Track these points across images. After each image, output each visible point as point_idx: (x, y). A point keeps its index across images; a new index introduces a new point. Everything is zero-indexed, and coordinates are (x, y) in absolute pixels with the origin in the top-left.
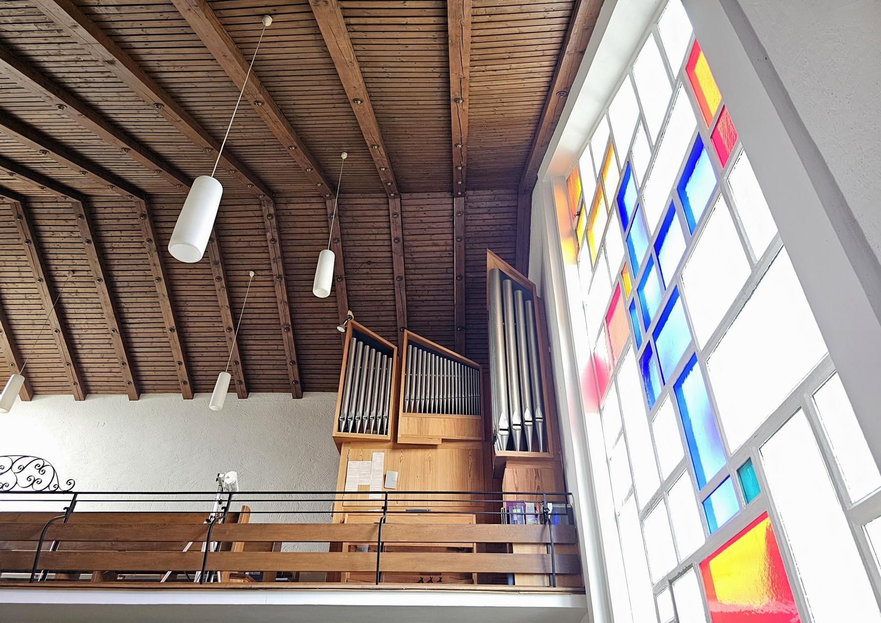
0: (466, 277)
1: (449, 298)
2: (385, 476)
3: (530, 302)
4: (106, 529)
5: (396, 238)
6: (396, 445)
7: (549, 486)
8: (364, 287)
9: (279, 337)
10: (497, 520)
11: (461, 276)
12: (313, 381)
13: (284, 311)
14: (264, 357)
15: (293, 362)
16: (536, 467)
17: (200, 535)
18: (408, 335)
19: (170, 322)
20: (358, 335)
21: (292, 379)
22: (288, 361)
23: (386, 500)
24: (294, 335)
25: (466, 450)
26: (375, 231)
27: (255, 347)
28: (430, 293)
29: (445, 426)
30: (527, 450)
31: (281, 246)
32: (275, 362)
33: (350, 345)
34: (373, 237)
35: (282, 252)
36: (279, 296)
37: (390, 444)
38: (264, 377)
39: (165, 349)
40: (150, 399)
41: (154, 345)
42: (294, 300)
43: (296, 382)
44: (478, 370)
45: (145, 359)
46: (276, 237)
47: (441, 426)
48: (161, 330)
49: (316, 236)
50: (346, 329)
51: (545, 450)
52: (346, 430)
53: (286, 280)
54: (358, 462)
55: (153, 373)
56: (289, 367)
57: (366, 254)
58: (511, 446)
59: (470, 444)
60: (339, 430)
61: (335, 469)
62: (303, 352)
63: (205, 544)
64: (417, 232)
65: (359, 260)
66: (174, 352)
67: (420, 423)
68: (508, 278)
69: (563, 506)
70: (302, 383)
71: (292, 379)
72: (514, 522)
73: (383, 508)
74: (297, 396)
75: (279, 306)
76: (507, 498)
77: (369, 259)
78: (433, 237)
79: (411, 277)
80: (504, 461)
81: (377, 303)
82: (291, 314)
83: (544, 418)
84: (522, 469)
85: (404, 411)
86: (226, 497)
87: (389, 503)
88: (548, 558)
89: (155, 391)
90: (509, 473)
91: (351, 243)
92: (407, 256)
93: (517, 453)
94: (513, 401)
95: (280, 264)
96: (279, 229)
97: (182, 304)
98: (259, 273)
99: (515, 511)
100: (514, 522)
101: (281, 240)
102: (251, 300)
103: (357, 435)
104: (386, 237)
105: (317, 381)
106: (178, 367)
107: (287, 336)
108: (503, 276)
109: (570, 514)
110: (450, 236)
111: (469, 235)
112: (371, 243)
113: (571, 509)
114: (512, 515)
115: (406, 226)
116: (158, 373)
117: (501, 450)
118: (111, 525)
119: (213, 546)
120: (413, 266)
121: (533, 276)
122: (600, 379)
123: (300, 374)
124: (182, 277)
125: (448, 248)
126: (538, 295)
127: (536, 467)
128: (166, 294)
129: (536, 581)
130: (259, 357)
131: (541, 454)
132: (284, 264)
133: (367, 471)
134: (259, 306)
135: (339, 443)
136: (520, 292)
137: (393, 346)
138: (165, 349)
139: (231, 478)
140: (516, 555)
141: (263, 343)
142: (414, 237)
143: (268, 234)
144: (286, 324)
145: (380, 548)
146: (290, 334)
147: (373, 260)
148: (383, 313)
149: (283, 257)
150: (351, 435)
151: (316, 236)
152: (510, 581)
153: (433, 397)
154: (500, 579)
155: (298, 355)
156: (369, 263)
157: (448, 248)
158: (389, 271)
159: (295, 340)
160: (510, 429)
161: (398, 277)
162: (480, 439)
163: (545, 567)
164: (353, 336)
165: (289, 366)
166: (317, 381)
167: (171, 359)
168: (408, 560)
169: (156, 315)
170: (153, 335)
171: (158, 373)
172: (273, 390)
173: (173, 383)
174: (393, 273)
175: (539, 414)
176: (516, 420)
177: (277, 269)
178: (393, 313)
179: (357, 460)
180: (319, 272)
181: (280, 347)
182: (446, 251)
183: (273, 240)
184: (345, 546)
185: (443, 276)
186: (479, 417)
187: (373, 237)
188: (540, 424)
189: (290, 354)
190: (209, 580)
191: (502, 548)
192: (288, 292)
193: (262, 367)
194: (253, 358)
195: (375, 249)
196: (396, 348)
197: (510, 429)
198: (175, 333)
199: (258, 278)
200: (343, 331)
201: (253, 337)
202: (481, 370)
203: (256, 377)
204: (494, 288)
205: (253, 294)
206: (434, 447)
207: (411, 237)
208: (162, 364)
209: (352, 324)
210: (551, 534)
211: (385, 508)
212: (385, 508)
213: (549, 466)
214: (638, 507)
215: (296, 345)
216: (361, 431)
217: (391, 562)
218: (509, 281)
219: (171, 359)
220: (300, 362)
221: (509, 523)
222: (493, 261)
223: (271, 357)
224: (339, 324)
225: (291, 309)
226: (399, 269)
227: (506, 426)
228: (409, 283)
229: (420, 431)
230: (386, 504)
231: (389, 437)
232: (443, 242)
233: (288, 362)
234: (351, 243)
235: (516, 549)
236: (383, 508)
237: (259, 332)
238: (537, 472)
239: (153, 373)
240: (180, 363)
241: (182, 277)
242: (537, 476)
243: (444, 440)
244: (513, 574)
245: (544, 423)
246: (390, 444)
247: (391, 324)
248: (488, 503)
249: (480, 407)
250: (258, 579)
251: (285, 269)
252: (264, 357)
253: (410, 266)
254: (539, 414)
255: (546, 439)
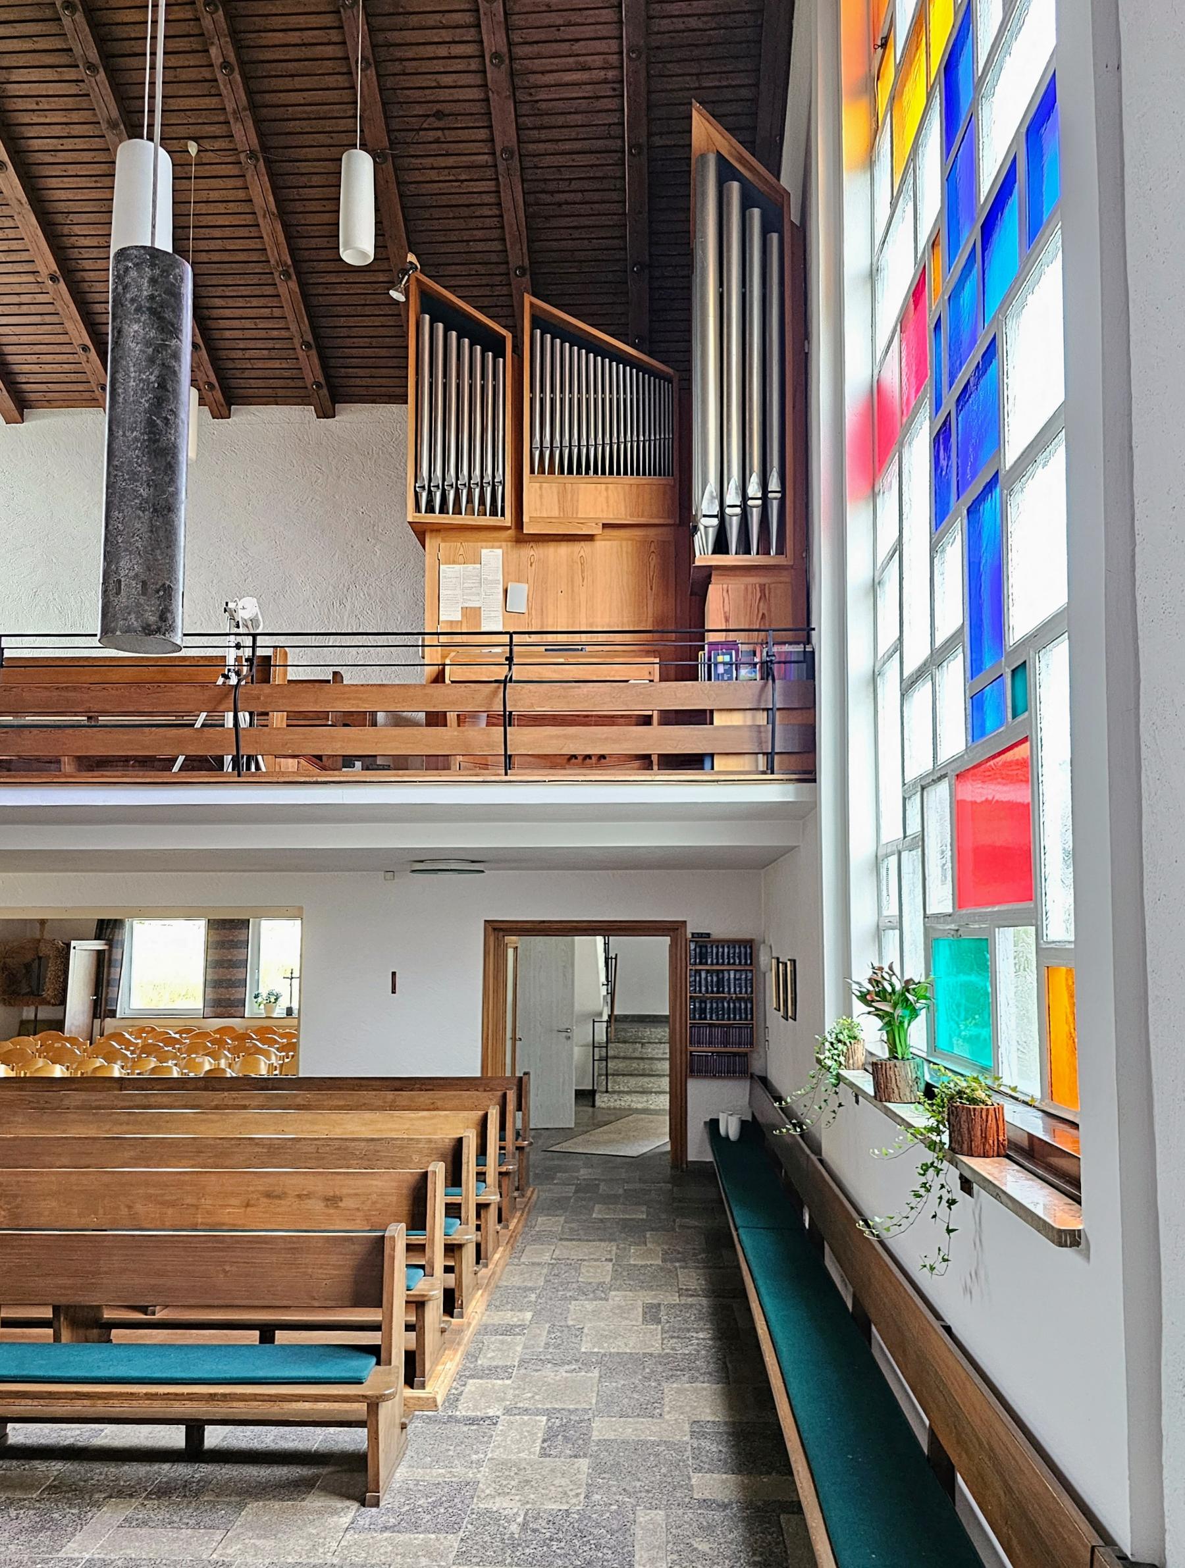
0: (650, 147)
1: (614, 196)
2: (506, 591)
3: (775, 236)
4: (64, 694)
5: (496, 55)
6: (521, 537)
7: (783, 617)
8: (433, 174)
9: (269, 290)
10: (690, 674)
11: (639, 146)
12: (352, 382)
13: (273, 233)
14: (248, 334)
15: (308, 346)
16: (763, 580)
17: (220, 702)
18: (532, 304)
19: (47, 263)
20: (433, 306)
21: (309, 380)
22: (297, 342)
23: (511, 644)
24: (302, 285)
25: (644, 542)
26: (446, 35)
27: (227, 313)
28: (575, 185)
29: (607, 498)
30: (748, 552)
31: (246, 78)
32: (270, 344)
33: (423, 334)
34: (442, 51)
35: (249, 93)
36: (258, 201)
37: (511, 532)
38: (254, 374)
39: (48, 319)
40: (46, 421)
41: (25, 309)
42: (291, 206)
43: (319, 385)
44: (670, 381)
45: (14, 339)
46: (232, 58)
47: (603, 499)
48: (31, 278)
49: (319, 51)
50: (407, 297)
51: (780, 551)
52: (430, 509)
53: (268, 162)
54: (457, 567)
55: (36, 368)
56: (301, 354)
57: (430, 95)
58: (721, 546)
59: (652, 532)
60: (418, 508)
61: (423, 594)
62: (324, 322)
63: (231, 714)
64: (541, 35)
65: (419, 110)
66: (69, 326)
67: (562, 495)
68: (736, 176)
69: (800, 648)
70: (332, 388)
71: (309, 380)
72: (718, 677)
73: (507, 659)
74: (325, 413)
75: (261, 221)
76: (711, 637)
77: (438, 106)
78: (578, 47)
79: (531, 147)
80: (708, 573)
81: (465, 212)
82: (288, 238)
83: (783, 491)
84: (737, 585)
85: (532, 472)
86: (248, 641)
87: (515, 649)
88: (766, 731)
89: (50, 403)
90: (715, 593)
91: (397, 67)
92: (521, 96)
93: (732, 559)
94: (729, 461)
95: (250, 123)
96: (235, 35)
97: (60, 218)
98: (207, 145)
99: (720, 659)
100: (718, 677)
101: (242, 63)
102: (203, 208)
103: (450, 519)
104: (470, 49)
105: (358, 382)
106: (82, 357)
107: (288, 288)
108: (726, 173)
109: (809, 661)
110: (614, 45)
111: (655, 41)
112: (438, 66)
113: (813, 653)
114: (716, 665)
115: (516, 20)
116: (48, 368)
117: (704, 555)
118: (75, 689)
119: (244, 718)
120: (538, 121)
121: (788, 180)
122: (881, 435)
123: (325, 367)
124: (48, 158)
125: (611, 74)
126: (795, 217)
127: (763, 580)
128: (24, 199)
129: (745, 763)
130: (238, 334)
131: (772, 559)
132: (257, 122)
133: (476, 585)
134: (221, 221)
135: (421, 532)
136: (756, 212)
137: (503, 332)
138: (48, 319)
139: (247, 609)
140: (718, 728)
141: (240, 302)
142: (536, 48)
143: (214, 51)
144: (280, 262)
145: (507, 720)
146: (294, 285)
147: (447, 108)
148: (479, 234)
149: (253, 107)
150: (443, 515)
151: (319, 51)
152: (707, 764)
153: (584, 442)
154: (694, 761)
155: (314, 328)
156: (439, 115)
157: (611, 74)
158: (483, 134)
159: (305, 296)
160: (721, 516)
161: (504, 150)
162: (670, 521)
163: (761, 743)
164: (423, 312)
165: (299, 350)
166: (358, 382)
167: (63, 338)
168: (551, 737)
169: (15, 245)
170: (18, 289)
171: (48, 368)
172: (275, 400)
173: (81, 387)
174: (492, 140)
175: (774, 484)
176: (732, 497)
177: (245, 135)
178: (495, 234)
179: (454, 563)
180: (347, 202)
181: (277, 312)
182: (606, 81)
183: (226, 65)
184: (452, 717)
185: (599, 144)
186: (669, 480)
187: (442, 51)
188: (775, 504)
189: (298, 327)
190: (248, 768)
191: (701, 717)
192: (275, 189)
193: (248, 354)
194: (228, 334)
195: (447, 80)
196: (510, 335)
197: (721, 516)
198: (62, 285)
199: (208, 157)
200: (402, 299)
201: (219, 291)
202: (676, 380)
203: (238, 374)
204: (704, 183)
205: (204, 195)
206: (590, 538)
207: (527, 50)
208: (50, 348)
209: (418, 280)
210: (777, 694)
211: (510, 659)
212: (510, 659)
213: (785, 577)
214: (932, 635)
215: (307, 307)
216: (457, 511)
217: (524, 739)
218: (735, 185)
219: (63, 338)
220: (321, 343)
221: (710, 679)
222: (704, 133)
223: (262, 334)
224: (392, 284)
225: (285, 226)
226: (505, 134)
227: (715, 510)
228: (528, 162)
229: (562, 508)
230: (511, 650)
231: (508, 520)
232: (598, 61)
233: (298, 346)
234: (397, 67)
235: (718, 719)
236: (507, 659)
237: (229, 280)
238: (762, 590)
239: (36, 368)
240: (85, 349)
241: (48, 158)
242: (763, 596)
243: (605, 526)
244: (712, 755)
245: (782, 501)
246: (511, 532)
247: (494, 258)
248: (680, 642)
249: (675, 467)
250: (328, 765)
251: (260, 135)
252: (248, 334)
253: (528, 121)
254: (774, 484)
255: (785, 531)
